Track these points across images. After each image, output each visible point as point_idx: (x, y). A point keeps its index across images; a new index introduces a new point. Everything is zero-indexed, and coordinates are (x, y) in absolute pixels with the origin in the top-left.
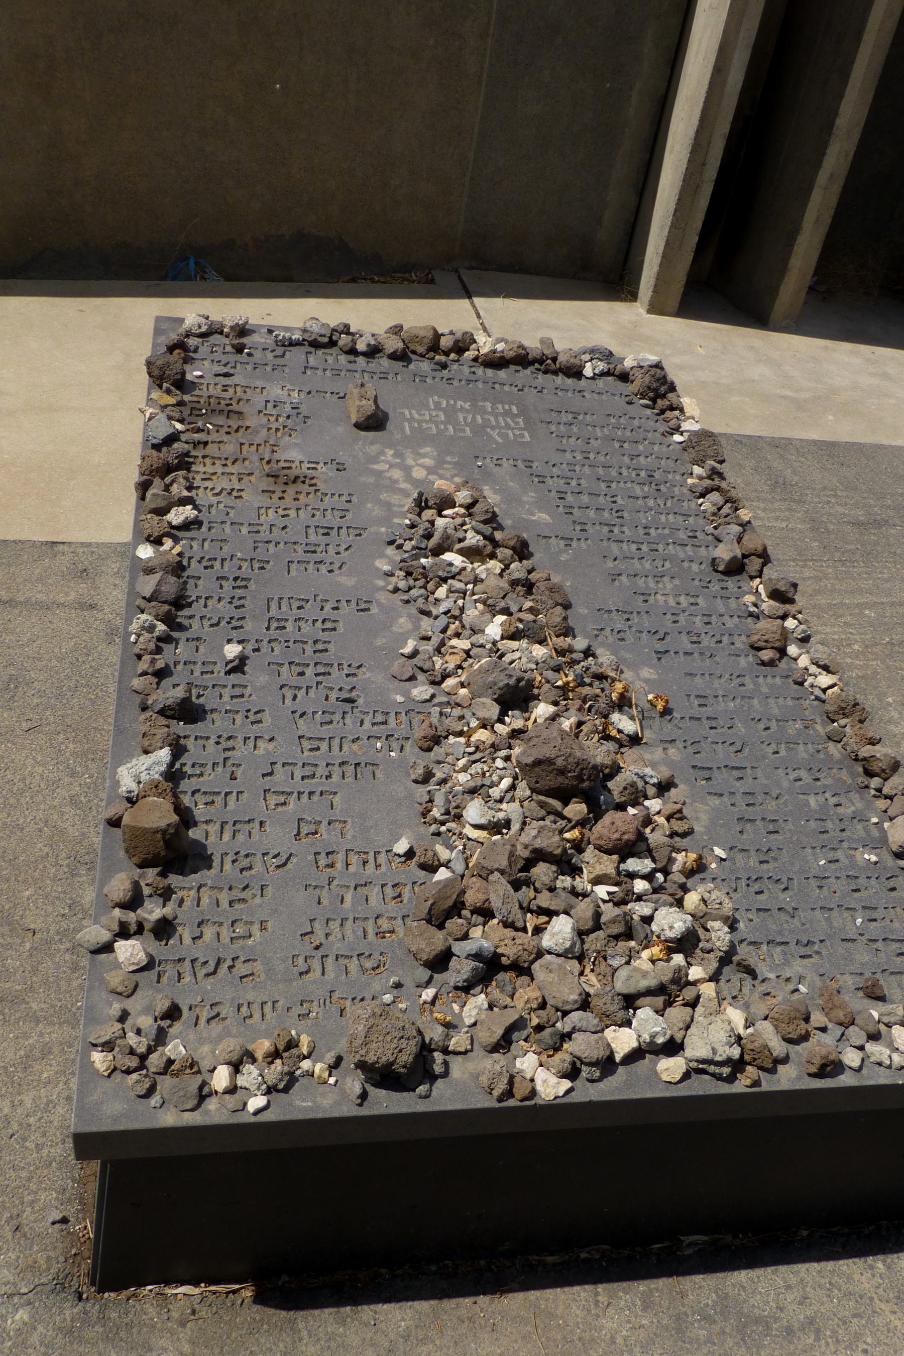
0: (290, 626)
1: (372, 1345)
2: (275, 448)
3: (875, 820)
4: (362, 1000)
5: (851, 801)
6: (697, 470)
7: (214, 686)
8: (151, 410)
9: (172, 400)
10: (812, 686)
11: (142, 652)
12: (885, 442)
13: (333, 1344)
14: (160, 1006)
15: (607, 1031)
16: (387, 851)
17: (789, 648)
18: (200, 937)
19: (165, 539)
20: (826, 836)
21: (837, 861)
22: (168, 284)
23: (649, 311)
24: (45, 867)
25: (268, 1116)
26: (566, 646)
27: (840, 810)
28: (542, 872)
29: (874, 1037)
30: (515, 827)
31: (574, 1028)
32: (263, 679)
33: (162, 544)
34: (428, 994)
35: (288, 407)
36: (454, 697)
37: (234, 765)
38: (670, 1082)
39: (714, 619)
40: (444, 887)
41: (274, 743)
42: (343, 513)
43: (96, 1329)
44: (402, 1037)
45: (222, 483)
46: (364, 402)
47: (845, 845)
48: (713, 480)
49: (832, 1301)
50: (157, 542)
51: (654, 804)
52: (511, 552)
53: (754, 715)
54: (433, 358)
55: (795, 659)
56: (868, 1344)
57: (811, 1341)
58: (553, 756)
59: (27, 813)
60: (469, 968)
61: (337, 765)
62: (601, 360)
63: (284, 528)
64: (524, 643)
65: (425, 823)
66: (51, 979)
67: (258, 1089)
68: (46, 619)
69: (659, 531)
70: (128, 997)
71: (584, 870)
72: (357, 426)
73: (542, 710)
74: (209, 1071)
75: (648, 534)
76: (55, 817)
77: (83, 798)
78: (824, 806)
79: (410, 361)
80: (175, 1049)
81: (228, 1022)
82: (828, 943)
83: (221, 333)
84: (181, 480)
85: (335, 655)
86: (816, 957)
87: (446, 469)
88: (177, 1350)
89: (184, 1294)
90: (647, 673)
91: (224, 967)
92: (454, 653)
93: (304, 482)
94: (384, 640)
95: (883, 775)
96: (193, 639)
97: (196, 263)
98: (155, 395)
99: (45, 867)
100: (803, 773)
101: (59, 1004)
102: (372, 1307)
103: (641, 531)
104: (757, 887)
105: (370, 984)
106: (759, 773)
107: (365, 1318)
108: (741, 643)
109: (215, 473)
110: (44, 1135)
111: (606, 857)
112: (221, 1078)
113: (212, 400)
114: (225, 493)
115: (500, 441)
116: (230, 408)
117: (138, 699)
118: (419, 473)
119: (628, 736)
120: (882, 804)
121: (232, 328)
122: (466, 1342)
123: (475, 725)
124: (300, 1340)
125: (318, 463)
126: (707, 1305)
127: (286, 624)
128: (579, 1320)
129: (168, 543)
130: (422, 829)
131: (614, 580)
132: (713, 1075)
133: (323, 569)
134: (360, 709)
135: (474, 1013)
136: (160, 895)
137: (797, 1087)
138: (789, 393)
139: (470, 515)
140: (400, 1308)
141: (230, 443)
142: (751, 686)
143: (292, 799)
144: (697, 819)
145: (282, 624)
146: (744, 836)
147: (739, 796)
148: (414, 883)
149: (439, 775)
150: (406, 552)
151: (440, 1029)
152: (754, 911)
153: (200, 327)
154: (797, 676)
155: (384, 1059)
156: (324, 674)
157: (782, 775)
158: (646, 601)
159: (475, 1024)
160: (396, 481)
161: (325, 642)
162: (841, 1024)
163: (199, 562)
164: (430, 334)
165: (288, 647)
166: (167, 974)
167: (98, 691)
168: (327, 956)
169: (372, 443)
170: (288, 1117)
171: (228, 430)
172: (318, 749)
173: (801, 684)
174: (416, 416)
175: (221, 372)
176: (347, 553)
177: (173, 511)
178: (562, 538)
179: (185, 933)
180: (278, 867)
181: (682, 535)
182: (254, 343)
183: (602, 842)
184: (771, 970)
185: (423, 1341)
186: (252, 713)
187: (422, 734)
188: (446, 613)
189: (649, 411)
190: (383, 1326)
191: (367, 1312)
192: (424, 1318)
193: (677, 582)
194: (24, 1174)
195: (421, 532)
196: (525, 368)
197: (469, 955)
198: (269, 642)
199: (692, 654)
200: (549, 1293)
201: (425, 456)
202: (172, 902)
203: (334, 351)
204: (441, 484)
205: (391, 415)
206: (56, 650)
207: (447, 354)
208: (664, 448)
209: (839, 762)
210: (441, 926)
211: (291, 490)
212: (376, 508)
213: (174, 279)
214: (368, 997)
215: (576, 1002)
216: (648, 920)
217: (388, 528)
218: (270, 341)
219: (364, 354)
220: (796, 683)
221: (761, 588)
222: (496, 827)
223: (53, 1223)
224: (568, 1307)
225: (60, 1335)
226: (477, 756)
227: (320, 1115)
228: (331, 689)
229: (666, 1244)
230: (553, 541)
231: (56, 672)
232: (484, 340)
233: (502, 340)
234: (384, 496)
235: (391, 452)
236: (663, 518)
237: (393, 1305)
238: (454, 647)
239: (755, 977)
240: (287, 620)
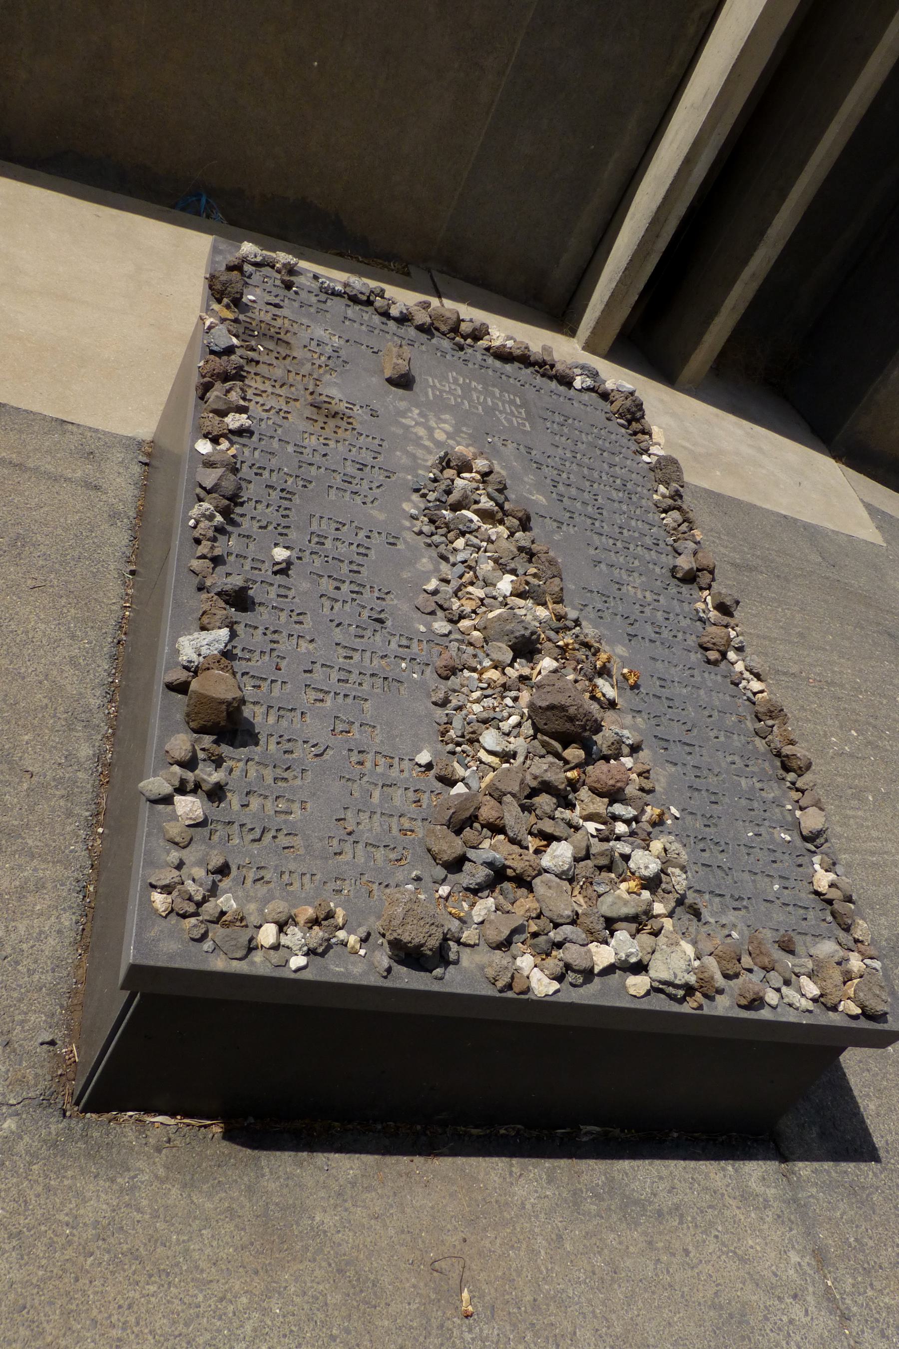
0: (328, 543)
1: (324, 1187)
2: (318, 383)
3: (789, 807)
4: (387, 886)
5: (772, 788)
6: (662, 488)
7: (262, 582)
8: (212, 320)
9: (231, 316)
10: (745, 688)
11: (201, 537)
12: (759, 503)
13: (291, 1183)
14: (214, 861)
15: (590, 946)
16: (410, 760)
17: (729, 653)
18: (247, 805)
19: (222, 440)
20: (752, 813)
21: (760, 835)
22: (177, 213)
23: (584, 349)
24: (43, 716)
25: (306, 975)
26: (563, 613)
27: (763, 794)
28: (545, 801)
29: (787, 983)
30: (520, 759)
31: (565, 939)
32: (305, 585)
33: (219, 444)
34: (444, 890)
35: (328, 349)
36: (468, 637)
37: (278, 656)
38: (635, 996)
39: (671, 616)
40: (466, 799)
41: (314, 645)
42: (376, 455)
43: (79, 1145)
44: (433, 924)
45: (271, 402)
46: (400, 361)
47: (767, 823)
48: (675, 501)
49: (693, 1193)
50: (215, 441)
51: (628, 761)
52: (517, 522)
53: (701, 703)
54: (454, 339)
55: (733, 664)
56: (719, 1231)
57: (676, 1224)
58: (567, 704)
59: (28, 663)
60: (484, 874)
61: (368, 675)
62: (588, 377)
63: (325, 455)
64: (529, 603)
65: (442, 741)
66: (47, 820)
67: (300, 949)
68: (53, 489)
69: (630, 533)
70: (184, 848)
71: (578, 806)
72: (390, 381)
73: (547, 663)
74: (255, 927)
75: (621, 533)
76: (55, 673)
77: (81, 661)
78: (752, 788)
79: (433, 336)
80: (227, 902)
81: (272, 885)
82: (753, 901)
83: (273, 267)
84: (238, 390)
85: (367, 578)
86: (744, 911)
87: (463, 438)
88: (152, 1172)
89: (161, 1123)
90: (620, 650)
91: (268, 837)
92: (471, 599)
93: (342, 419)
94: (409, 575)
95: (799, 772)
96: (244, 536)
97: (207, 202)
98: (216, 306)
99: (43, 716)
100: (736, 758)
101: (54, 844)
102: (326, 1155)
103: (617, 530)
104: (701, 845)
105: (394, 873)
106: (704, 751)
107: (319, 1163)
108: (692, 641)
109: (265, 391)
110: (36, 962)
111: (598, 799)
112: (268, 934)
113: (263, 325)
114: (273, 411)
115: (506, 425)
116: (279, 336)
117: (196, 581)
118: (440, 436)
119: (608, 700)
120: (795, 795)
121: (284, 265)
122: (403, 1194)
123: (488, 664)
124: (263, 1175)
125: (354, 405)
126: (598, 1185)
127: (325, 542)
128: (497, 1185)
129: (224, 444)
130: (440, 746)
131: (596, 566)
132: (669, 996)
133: (358, 500)
134: (388, 630)
135: (483, 913)
136: (213, 761)
137: (730, 1015)
138: (687, 445)
139: (484, 482)
140: (349, 1158)
141: (279, 367)
142: (699, 679)
143: (329, 699)
144: (658, 780)
145: (322, 540)
146: (692, 802)
147: (689, 767)
148: (432, 792)
149: (454, 702)
150: (429, 502)
151: (457, 923)
152: (700, 865)
153: (256, 256)
154: (735, 678)
155: (417, 940)
156: (357, 593)
157: (721, 757)
158: (620, 589)
159: (482, 922)
160: (421, 438)
161: (359, 565)
162: (764, 968)
163: (250, 467)
164: (454, 317)
165: (327, 562)
166: (218, 833)
167: (99, 566)
168: (357, 842)
169: (401, 399)
170: (323, 979)
171: (278, 355)
172: (351, 658)
173: (737, 685)
174: (438, 385)
175: (273, 302)
176: (378, 491)
177: (231, 416)
178: (555, 520)
179: (234, 800)
180: (316, 755)
181: (648, 541)
182: (300, 284)
183: (596, 785)
184: (712, 916)
185: (368, 1189)
186: (295, 613)
187: (444, 663)
188: (463, 562)
189: (623, 430)
190: (334, 1171)
191: (321, 1158)
192: (369, 1170)
193: (644, 579)
194: (15, 995)
195: (443, 487)
196: (526, 367)
197: (484, 862)
198: (311, 553)
199: (655, 642)
200: (473, 1161)
201: (445, 422)
202: (223, 768)
203: (370, 309)
204: (462, 449)
205: (417, 379)
206: (62, 520)
207: (465, 338)
208: (635, 465)
209: (764, 754)
210: (458, 832)
211: (332, 423)
212: (404, 457)
213: (183, 209)
214: (393, 884)
215: (569, 917)
216: (626, 858)
217: (413, 476)
218: (315, 285)
219: (395, 319)
220: (733, 683)
221: (709, 599)
222: (507, 756)
223: (42, 1044)
224: (487, 1174)
225: (45, 1147)
226: (489, 692)
227: (351, 981)
228: (364, 607)
229: (568, 1130)
230: (548, 520)
231: (61, 541)
232: (498, 334)
233: (511, 338)
234: (410, 448)
235: (417, 411)
236: (633, 523)
237: (343, 1155)
238: (471, 594)
239: (699, 920)
240: (326, 538)
